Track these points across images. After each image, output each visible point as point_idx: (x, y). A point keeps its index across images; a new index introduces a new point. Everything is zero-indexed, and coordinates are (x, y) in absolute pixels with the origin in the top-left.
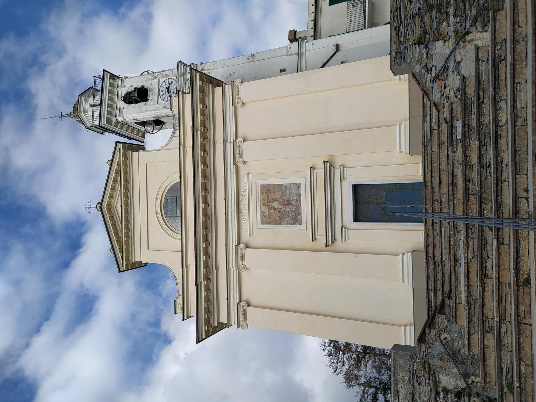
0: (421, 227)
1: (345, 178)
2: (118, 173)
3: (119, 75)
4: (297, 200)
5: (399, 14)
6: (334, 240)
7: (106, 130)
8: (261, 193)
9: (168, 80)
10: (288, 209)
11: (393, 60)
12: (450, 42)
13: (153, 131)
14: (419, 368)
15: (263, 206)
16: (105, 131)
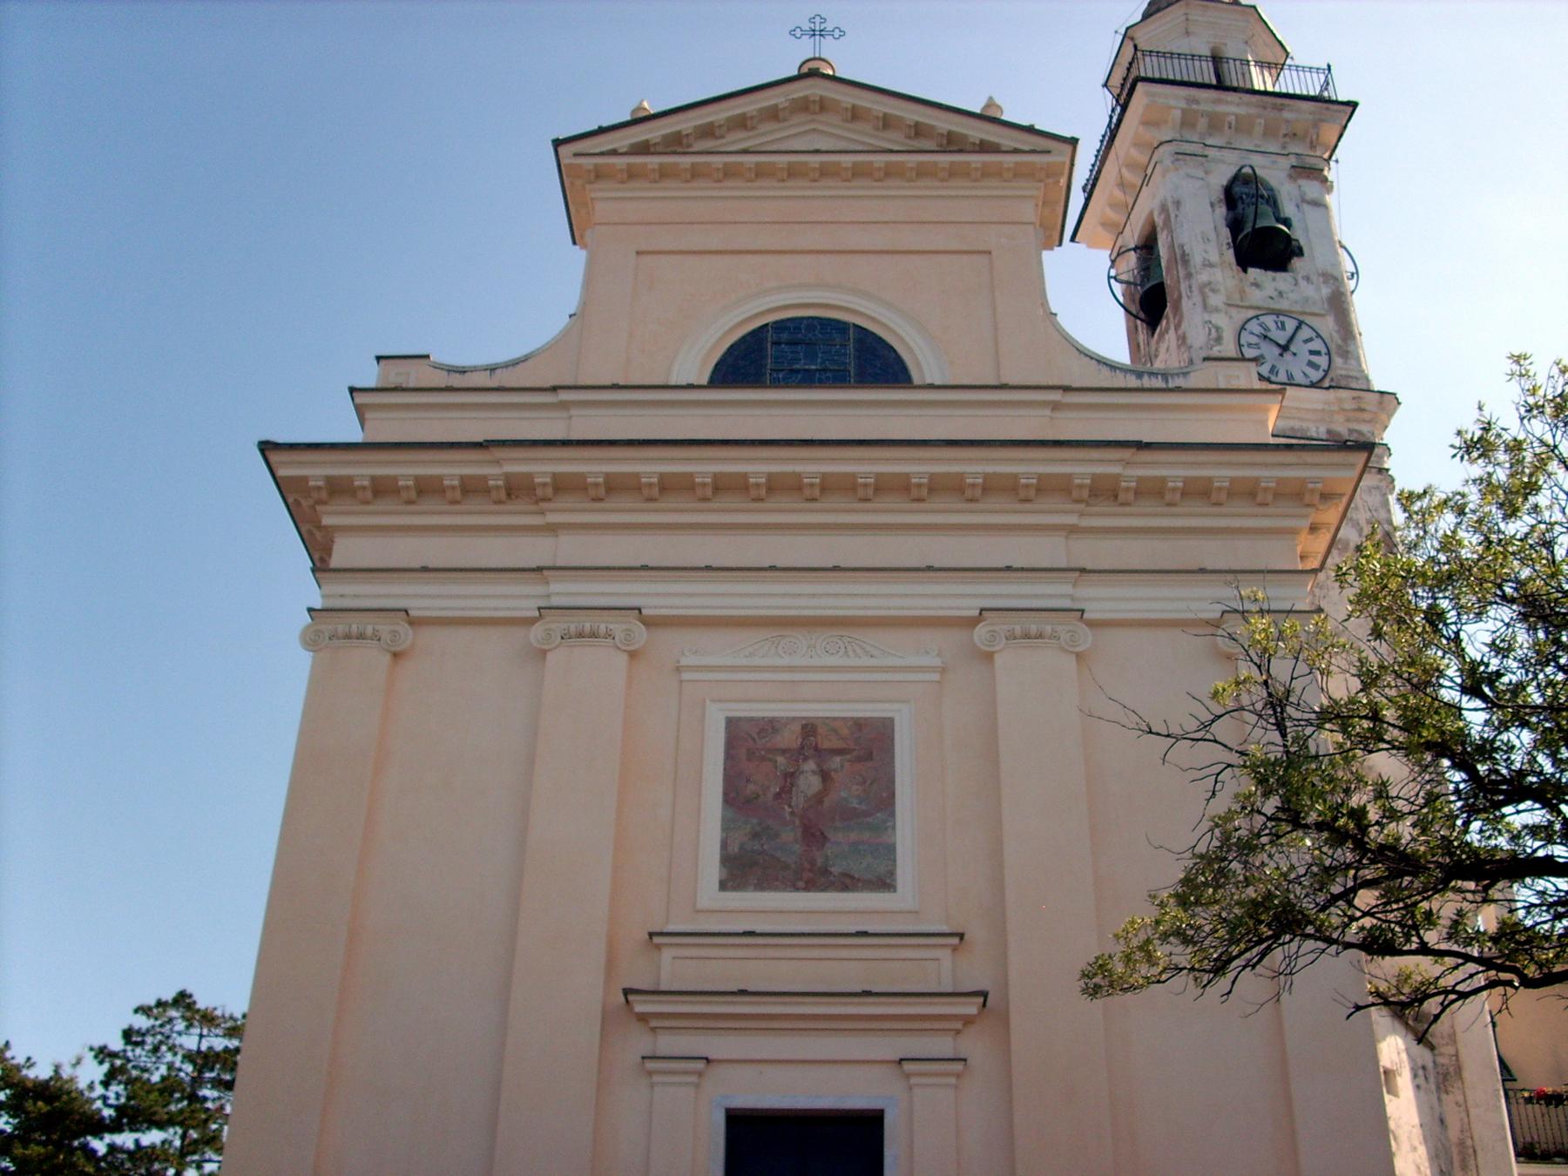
3: (1337, 161)
6: (654, 1023)
15: (804, 727)
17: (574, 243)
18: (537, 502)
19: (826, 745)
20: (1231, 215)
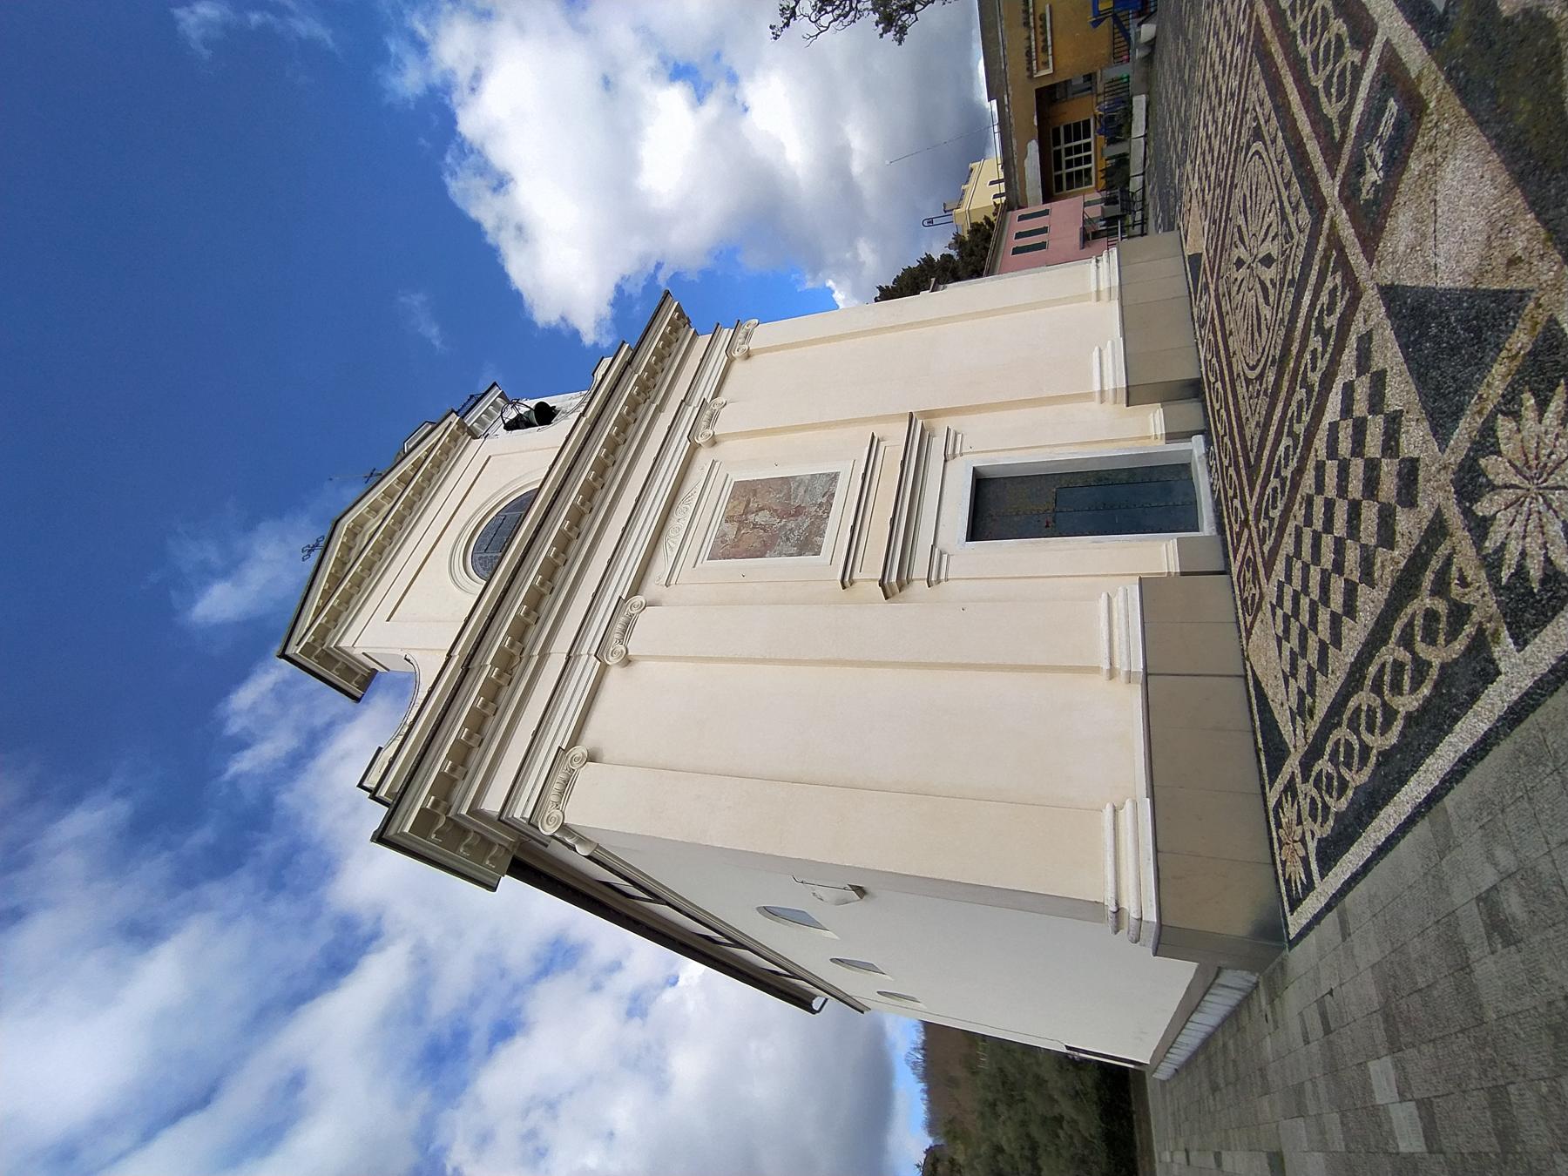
1: (957, 452)
4: (820, 505)
10: (792, 525)
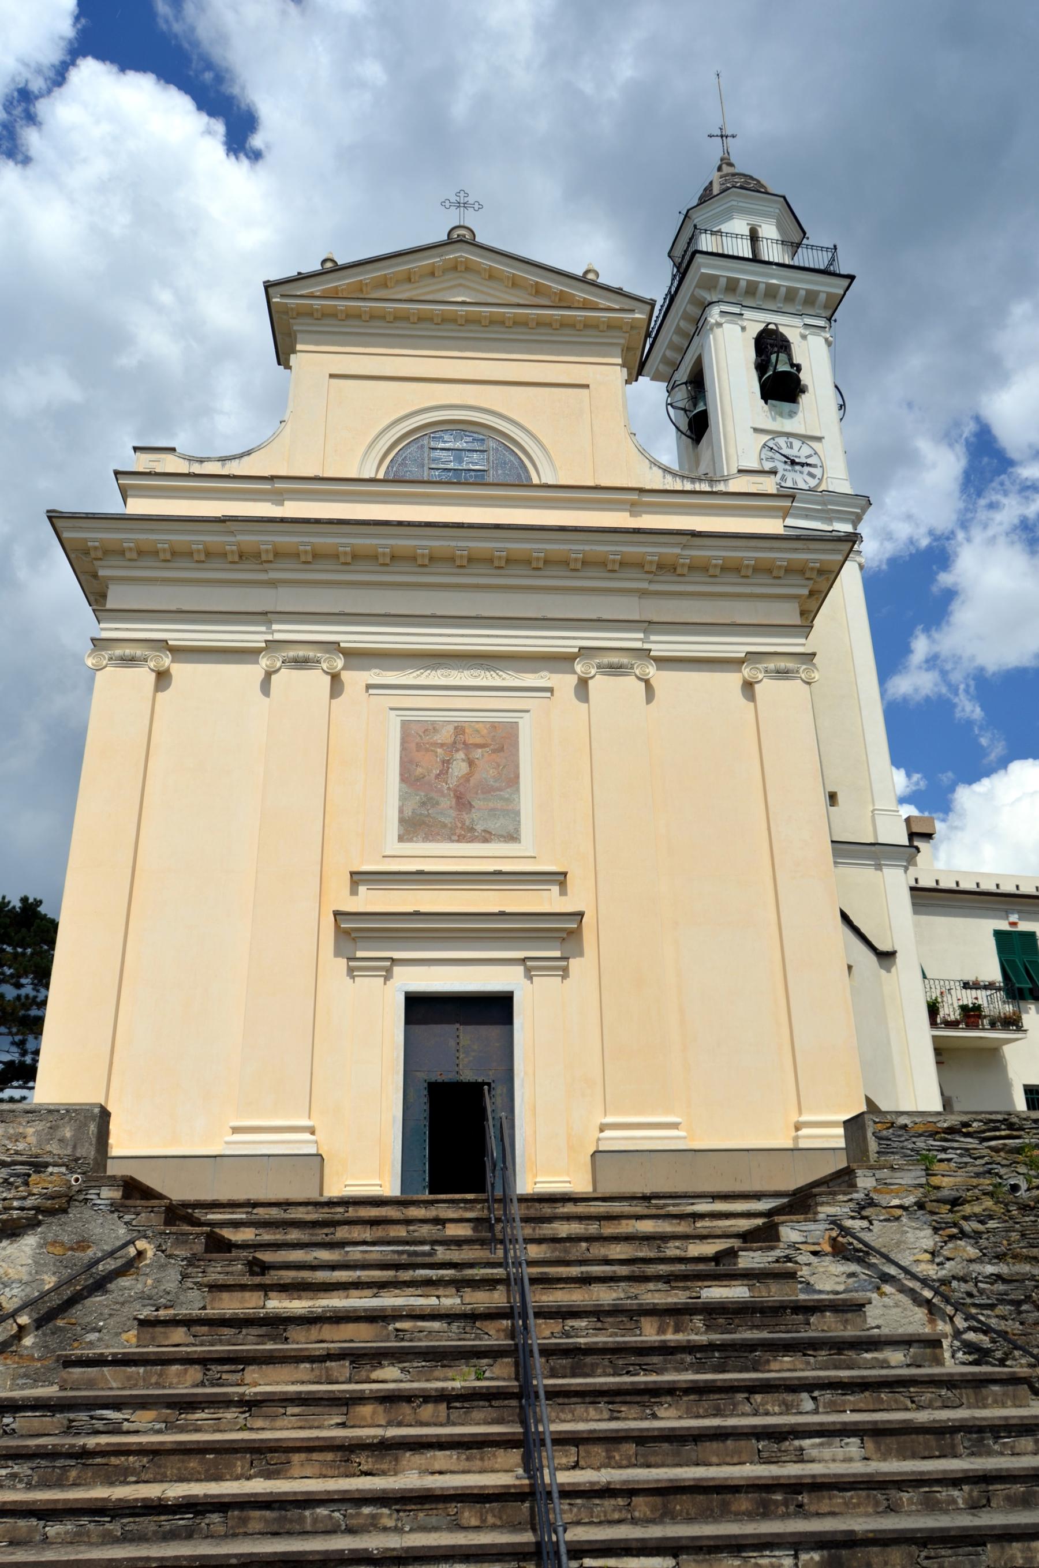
0: (389, 1186)
2: (563, 302)
3: (835, 321)
5: (1003, 1133)
6: (353, 935)
7: (682, 271)
8: (494, 726)
9: (819, 464)
11: (888, 1117)
12: (930, 1267)
13: (672, 406)
14: (51, 1182)
15: (456, 728)
16: (678, 266)
17: (279, 364)
18: (261, 563)
19: (471, 741)
20: (759, 359)
